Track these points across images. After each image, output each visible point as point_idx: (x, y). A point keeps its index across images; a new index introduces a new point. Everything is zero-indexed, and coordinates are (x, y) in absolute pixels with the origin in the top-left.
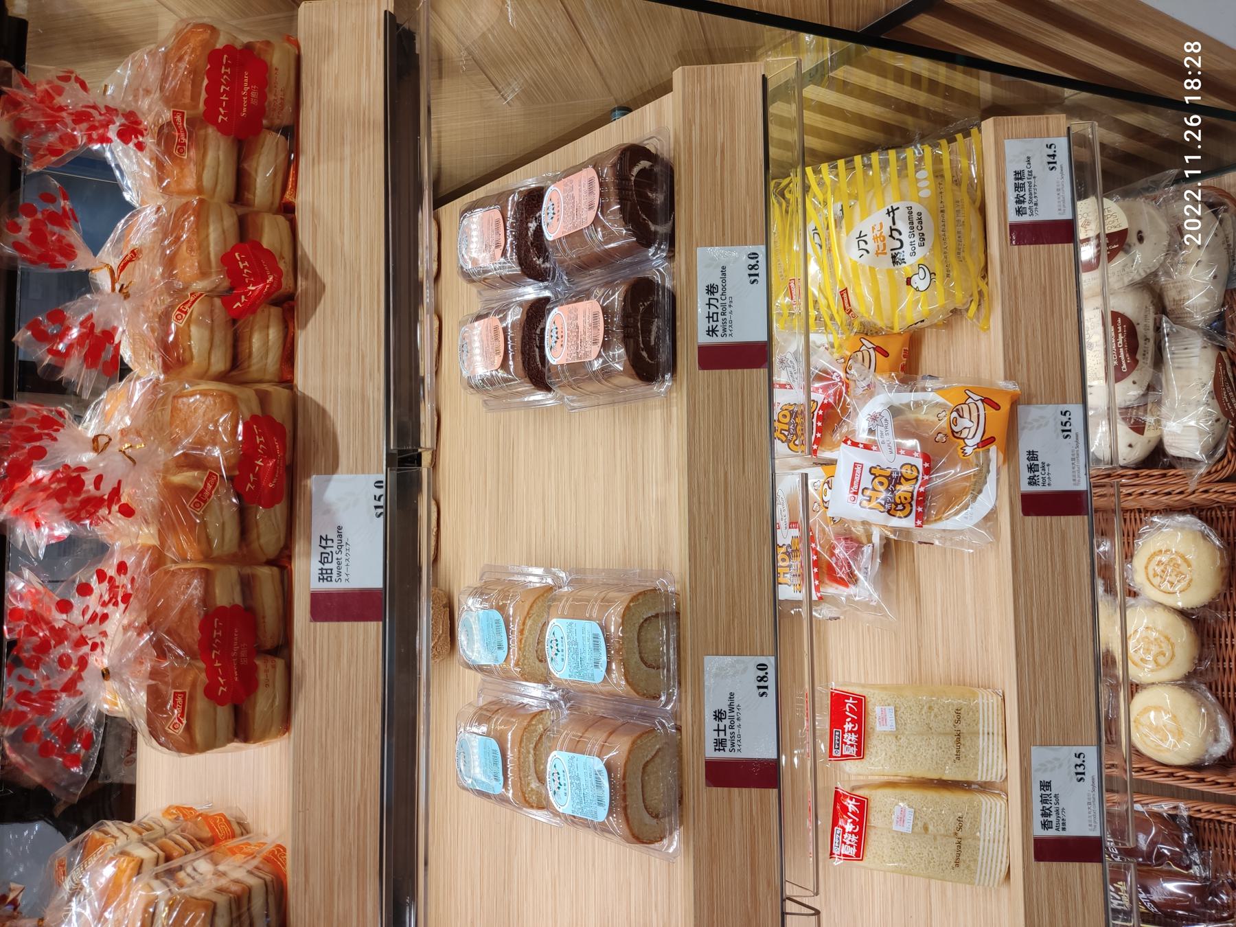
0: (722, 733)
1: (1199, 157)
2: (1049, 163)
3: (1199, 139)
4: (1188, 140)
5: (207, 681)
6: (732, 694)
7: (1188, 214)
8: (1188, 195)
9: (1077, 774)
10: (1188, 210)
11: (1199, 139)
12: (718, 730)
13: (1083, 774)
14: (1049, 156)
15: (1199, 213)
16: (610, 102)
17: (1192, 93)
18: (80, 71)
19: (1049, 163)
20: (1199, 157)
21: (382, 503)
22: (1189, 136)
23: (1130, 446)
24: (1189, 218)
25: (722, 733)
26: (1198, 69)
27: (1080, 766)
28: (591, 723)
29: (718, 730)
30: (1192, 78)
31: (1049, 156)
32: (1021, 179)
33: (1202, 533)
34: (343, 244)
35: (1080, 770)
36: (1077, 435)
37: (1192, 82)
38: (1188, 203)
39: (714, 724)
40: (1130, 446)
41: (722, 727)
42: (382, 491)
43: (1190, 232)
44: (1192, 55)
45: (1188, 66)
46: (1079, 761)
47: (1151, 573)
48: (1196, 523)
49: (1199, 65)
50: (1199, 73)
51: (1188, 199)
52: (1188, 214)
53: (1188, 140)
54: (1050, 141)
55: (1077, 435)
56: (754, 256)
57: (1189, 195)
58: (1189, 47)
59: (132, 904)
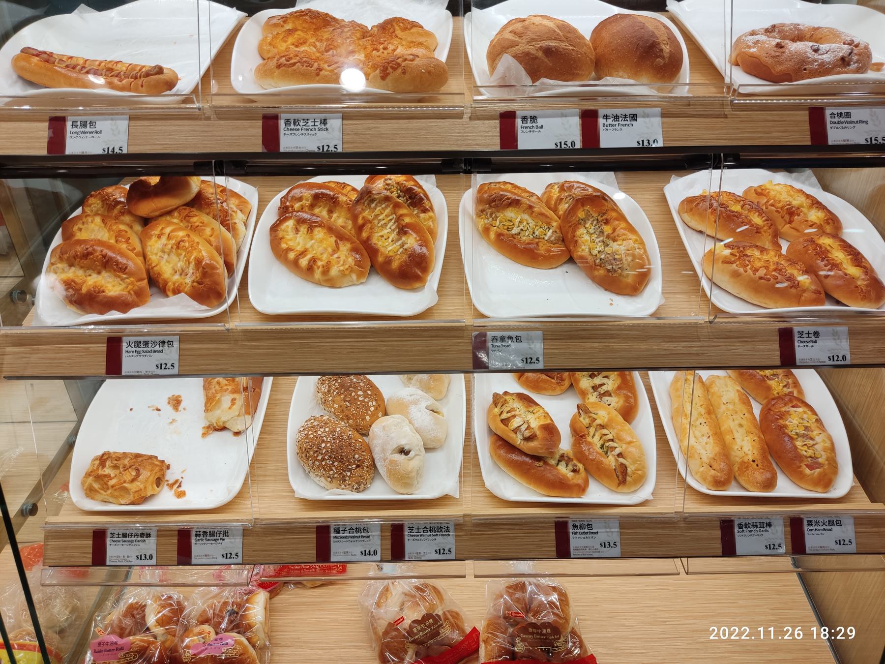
2: (365, 551)
3: (786, 637)
4: (785, 629)
8: (745, 629)
9: (141, 555)
10: (735, 630)
12: (808, 334)
13: (141, 559)
14: (370, 551)
15: (732, 637)
19: (365, 551)
24: (729, 630)
26: (836, 637)
27: (609, 545)
29: (808, 334)
31: (370, 551)
32: (430, 530)
35: (607, 545)
37: (826, 633)
38: (740, 629)
39: (812, 331)
41: (810, 335)
42: (569, 145)
43: (719, 630)
44: (730, 634)
45: (838, 630)
46: (612, 545)
49: (838, 638)
50: (833, 638)
51: (742, 629)
53: (785, 629)
54: (618, 544)
56: (844, 358)
57: (745, 630)
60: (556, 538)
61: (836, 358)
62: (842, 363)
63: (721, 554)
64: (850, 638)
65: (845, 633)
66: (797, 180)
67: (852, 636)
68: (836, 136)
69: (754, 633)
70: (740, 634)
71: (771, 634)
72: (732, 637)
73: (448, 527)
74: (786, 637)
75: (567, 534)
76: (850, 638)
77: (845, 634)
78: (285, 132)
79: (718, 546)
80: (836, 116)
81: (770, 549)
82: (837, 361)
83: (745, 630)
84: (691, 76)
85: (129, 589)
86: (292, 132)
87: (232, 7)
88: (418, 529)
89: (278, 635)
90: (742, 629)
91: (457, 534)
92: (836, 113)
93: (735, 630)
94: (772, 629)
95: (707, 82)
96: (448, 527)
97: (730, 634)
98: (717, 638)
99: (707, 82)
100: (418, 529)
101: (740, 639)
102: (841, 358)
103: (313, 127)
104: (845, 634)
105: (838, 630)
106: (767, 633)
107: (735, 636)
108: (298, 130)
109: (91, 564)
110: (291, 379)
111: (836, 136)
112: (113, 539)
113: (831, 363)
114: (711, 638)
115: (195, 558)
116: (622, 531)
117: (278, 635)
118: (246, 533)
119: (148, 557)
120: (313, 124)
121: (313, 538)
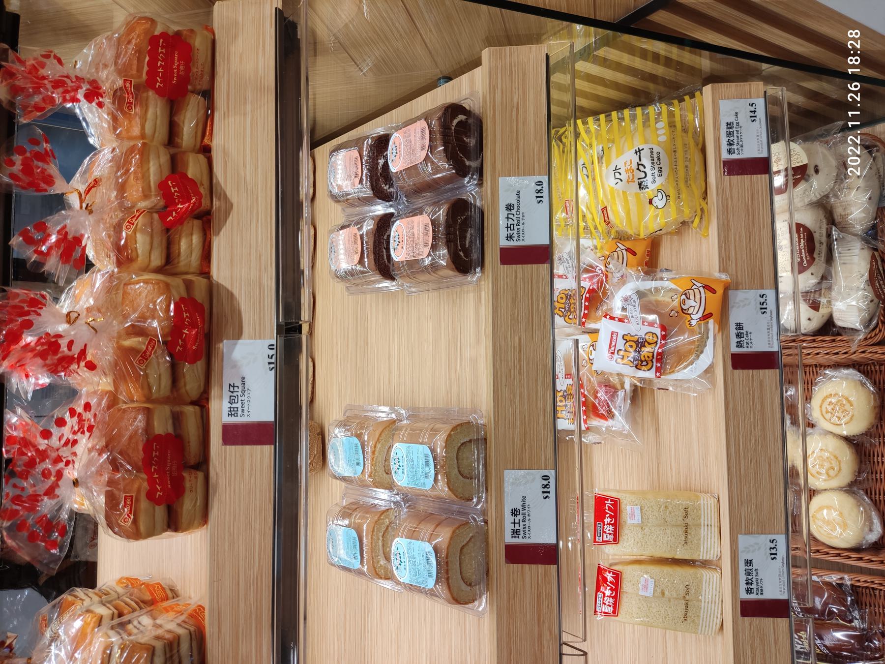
0: (517, 525)
1: (859, 113)
2: (751, 117)
3: (858, 99)
4: (851, 100)
6: (524, 497)
7: (850, 153)
8: (851, 140)
9: (771, 554)
10: (851, 150)
11: (858, 99)
12: (514, 523)
13: (776, 554)
14: (751, 112)
15: (859, 153)
16: (437, 73)
17: (854, 66)
18: (57, 51)
19: (751, 117)
20: (859, 113)
22: (851, 97)
23: (809, 319)
24: (851, 156)
25: (517, 525)
26: (858, 50)
27: (773, 548)
28: (423, 518)
29: (514, 523)
30: (853, 56)
31: (751, 112)
32: (731, 128)
33: (861, 382)
34: (245, 175)
35: (773, 551)
36: (771, 312)
37: (854, 59)
38: (850, 145)
39: (511, 519)
40: (809, 319)
41: (517, 521)
43: (852, 166)
44: (853, 39)
45: (850, 47)
46: (772, 545)
47: (824, 410)
48: (857, 375)
49: (858, 47)
50: (859, 52)
51: (851, 143)
52: (850, 153)
53: (851, 100)
54: (752, 101)
55: (771, 312)
57: (851, 140)
58: (851, 34)
59: (95, 648)
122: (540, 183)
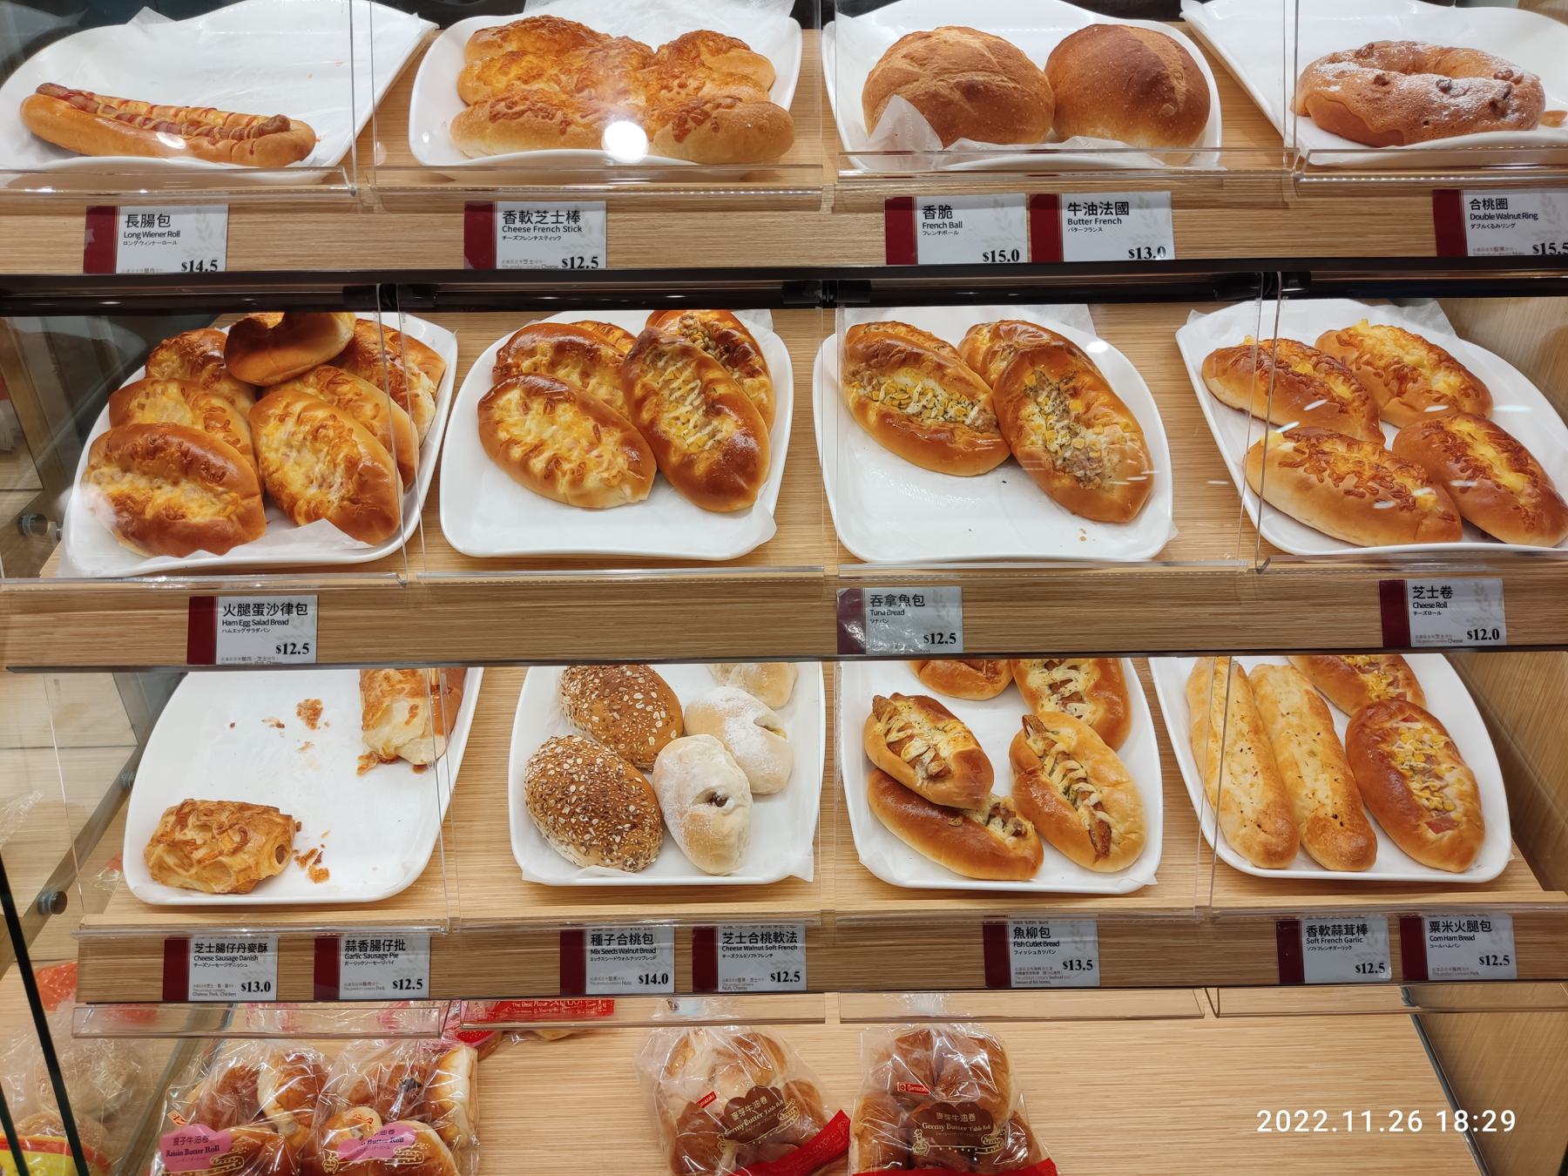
2: (647, 976)
3: (1392, 1129)
4: (1391, 1115)
5: (146, 9)
8: (1321, 1115)
9: (250, 984)
10: (1302, 1116)
12: (1432, 591)
13: (250, 990)
14: (655, 976)
15: (1298, 1129)
19: (647, 976)
21: (1548, 251)
24: (1292, 1115)
26: (1480, 1128)
27: (1079, 965)
29: (1432, 591)
31: (655, 976)
32: (762, 939)
35: (1075, 965)
37: (1464, 1121)
38: (1311, 1114)
39: (1438, 586)
41: (1435, 594)
43: (1273, 1116)
44: (1294, 1123)
45: (1484, 1115)
46: (1084, 965)
49: (1485, 1129)
50: (1476, 1130)
51: (1315, 1115)
53: (1391, 1115)
54: (1095, 963)
57: (1320, 1116)
60: (985, 953)
61: (1481, 634)
62: (1492, 642)
63: (1277, 981)
64: (1506, 1130)
65: (1498, 1121)
66: (1412, 318)
67: (1509, 1126)
68: (1481, 240)
69: (1337, 1121)
70: (1312, 1123)
71: (1365, 1124)
72: (1298, 1129)
73: (793, 934)
74: (1392, 1129)
75: (1004, 945)
76: (1506, 1130)
77: (1498, 1124)
78: (505, 234)
79: (1272, 966)
80: (1481, 205)
81: (1364, 972)
82: (1483, 639)
83: (1320, 1116)
84: (1224, 134)
85: (228, 1043)
86: (518, 233)
87: (411, 12)
88: (741, 937)
89: (492, 1125)
90: (1315, 1115)
91: (809, 946)
92: (1481, 200)
93: (1302, 1116)
94: (1368, 1114)
95: (1253, 145)
96: (793, 934)
97: (1294, 1123)
98: (1270, 1130)
99: (1253, 145)
100: (741, 937)
101: (1312, 1131)
102: (1489, 635)
103: (554, 225)
104: (1498, 1124)
105: (1484, 1115)
106: (1359, 1121)
107: (1302, 1127)
108: (528, 230)
109: (161, 999)
110: (516, 671)
111: (1481, 240)
112: (201, 955)
113: (1473, 642)
114: (1261, 1129)
115: (346, 989)
116: (1102, 940)
117: (492, 1125)
118: (436, 943)
119: (262, 987)
120: (554, 219)
121: (554, 952)
122: (1496, 634)
